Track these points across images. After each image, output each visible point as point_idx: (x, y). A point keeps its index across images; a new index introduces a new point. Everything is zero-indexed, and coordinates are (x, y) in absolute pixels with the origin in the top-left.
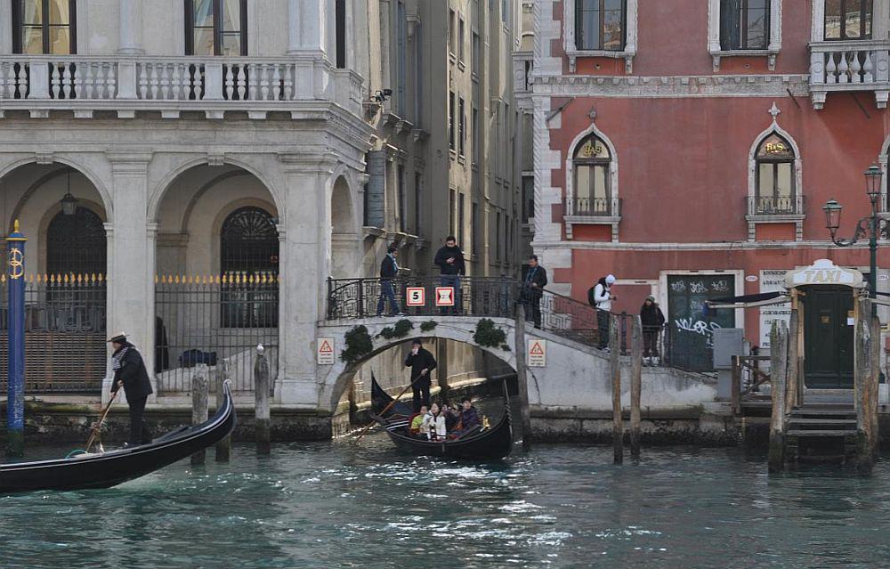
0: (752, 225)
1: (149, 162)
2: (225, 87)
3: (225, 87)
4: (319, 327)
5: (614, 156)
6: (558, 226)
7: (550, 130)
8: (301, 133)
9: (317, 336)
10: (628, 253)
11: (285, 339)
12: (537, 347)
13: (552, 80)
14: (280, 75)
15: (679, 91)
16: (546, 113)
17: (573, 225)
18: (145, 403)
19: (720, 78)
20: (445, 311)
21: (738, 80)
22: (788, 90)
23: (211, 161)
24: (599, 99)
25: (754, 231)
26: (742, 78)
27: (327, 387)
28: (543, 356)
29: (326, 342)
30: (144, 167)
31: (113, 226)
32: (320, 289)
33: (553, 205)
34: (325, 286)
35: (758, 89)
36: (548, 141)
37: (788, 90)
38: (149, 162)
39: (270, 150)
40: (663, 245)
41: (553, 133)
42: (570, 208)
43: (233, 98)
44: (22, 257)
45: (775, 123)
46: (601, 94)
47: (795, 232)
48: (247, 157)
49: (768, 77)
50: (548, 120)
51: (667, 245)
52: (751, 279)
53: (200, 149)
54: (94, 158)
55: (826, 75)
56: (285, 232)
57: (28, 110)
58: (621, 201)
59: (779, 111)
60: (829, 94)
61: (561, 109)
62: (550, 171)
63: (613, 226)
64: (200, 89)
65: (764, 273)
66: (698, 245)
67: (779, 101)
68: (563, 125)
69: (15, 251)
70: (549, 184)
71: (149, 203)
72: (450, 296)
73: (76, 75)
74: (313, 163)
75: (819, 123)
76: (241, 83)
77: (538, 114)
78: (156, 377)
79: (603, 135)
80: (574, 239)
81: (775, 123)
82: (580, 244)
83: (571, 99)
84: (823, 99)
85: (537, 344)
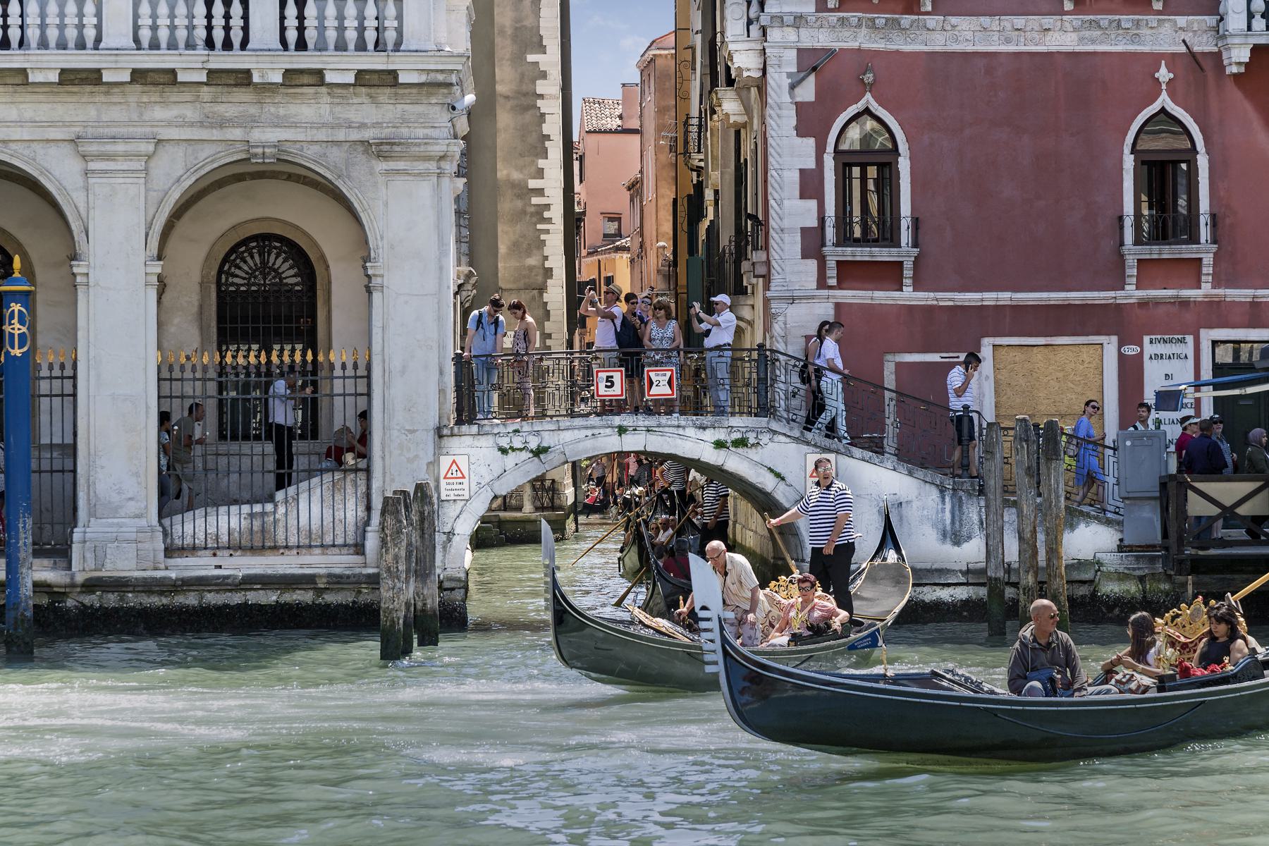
0: (1131, 261)
1: (149, 157)
2: (283, 29)
3: (283, 29)
4: (441, 437)
5: (903, 147)
6: (812, 265)
7: (796, 103)
8: (407, 107)
9: (439, 451)
10: (930, 310)
11: (383, 458)
12: (454, 468)
13: (799, 21)
14: (318, 9)
15: (1008, 41)
16: (789, 75)
17: (838, 262)
18: (850, 563)
19: (1076, 20)
20: (664, 407)
21: (1104, 23)
22: (1184, 41)
23: (255, 155)
24: (877, 53)
25: (1135, 272)
26: (1111, 22)
27: (456, 539)
28: (465, 481)
29: (454, 461)
30: (139, 165)
31: (88, 266)
32: (441, 373)
33: (802, 229)
34: (450, 369)
35: (1136, 38)
36: (794, 122)
37: (1184, 41)
38: (149, 157)
39: (355, 135)
40: (987, 295)
41: (800, 107)
42: (830, 233)
43: (297, 49)
44: (28, 318)
45: (1164, 95)
46: (880, 45)
47: (1199, 274)
48: (316, 148)
49: (1153, 20)
50: (793, 87)
51: (993, 295)
52: (1131, 350)
53: (237, 134)
54: (53, 150)
55: (1250, 16)
56: (382, 276)
57: (25, 70)
58: (1213, 216)
59: (1171, 76)
60: (1256, 49)
61: (814, 69)
62: (797, 175)
63: (1205, 262)
64: (241, 33)
65: (1151, 342)
66: (1045, 295)
67: (1172, 59)
68: (818, 93)
69: (16, 307)
70: (797, 193)
71: (149, 226)
72: (670, 383)
73: (307, 13)
74: (428, 158)
75: (1235, 95)
76: (237, 22)
77: (776, 76)
78: (161, 524)
79: (885, 112)
80: (840, 286)
81: (1164, 95)
82: (850, 296)
83: (830, 53)
84: (1243, 55)
85: (454, 461)
